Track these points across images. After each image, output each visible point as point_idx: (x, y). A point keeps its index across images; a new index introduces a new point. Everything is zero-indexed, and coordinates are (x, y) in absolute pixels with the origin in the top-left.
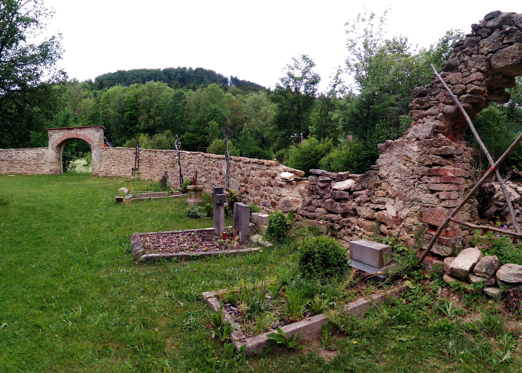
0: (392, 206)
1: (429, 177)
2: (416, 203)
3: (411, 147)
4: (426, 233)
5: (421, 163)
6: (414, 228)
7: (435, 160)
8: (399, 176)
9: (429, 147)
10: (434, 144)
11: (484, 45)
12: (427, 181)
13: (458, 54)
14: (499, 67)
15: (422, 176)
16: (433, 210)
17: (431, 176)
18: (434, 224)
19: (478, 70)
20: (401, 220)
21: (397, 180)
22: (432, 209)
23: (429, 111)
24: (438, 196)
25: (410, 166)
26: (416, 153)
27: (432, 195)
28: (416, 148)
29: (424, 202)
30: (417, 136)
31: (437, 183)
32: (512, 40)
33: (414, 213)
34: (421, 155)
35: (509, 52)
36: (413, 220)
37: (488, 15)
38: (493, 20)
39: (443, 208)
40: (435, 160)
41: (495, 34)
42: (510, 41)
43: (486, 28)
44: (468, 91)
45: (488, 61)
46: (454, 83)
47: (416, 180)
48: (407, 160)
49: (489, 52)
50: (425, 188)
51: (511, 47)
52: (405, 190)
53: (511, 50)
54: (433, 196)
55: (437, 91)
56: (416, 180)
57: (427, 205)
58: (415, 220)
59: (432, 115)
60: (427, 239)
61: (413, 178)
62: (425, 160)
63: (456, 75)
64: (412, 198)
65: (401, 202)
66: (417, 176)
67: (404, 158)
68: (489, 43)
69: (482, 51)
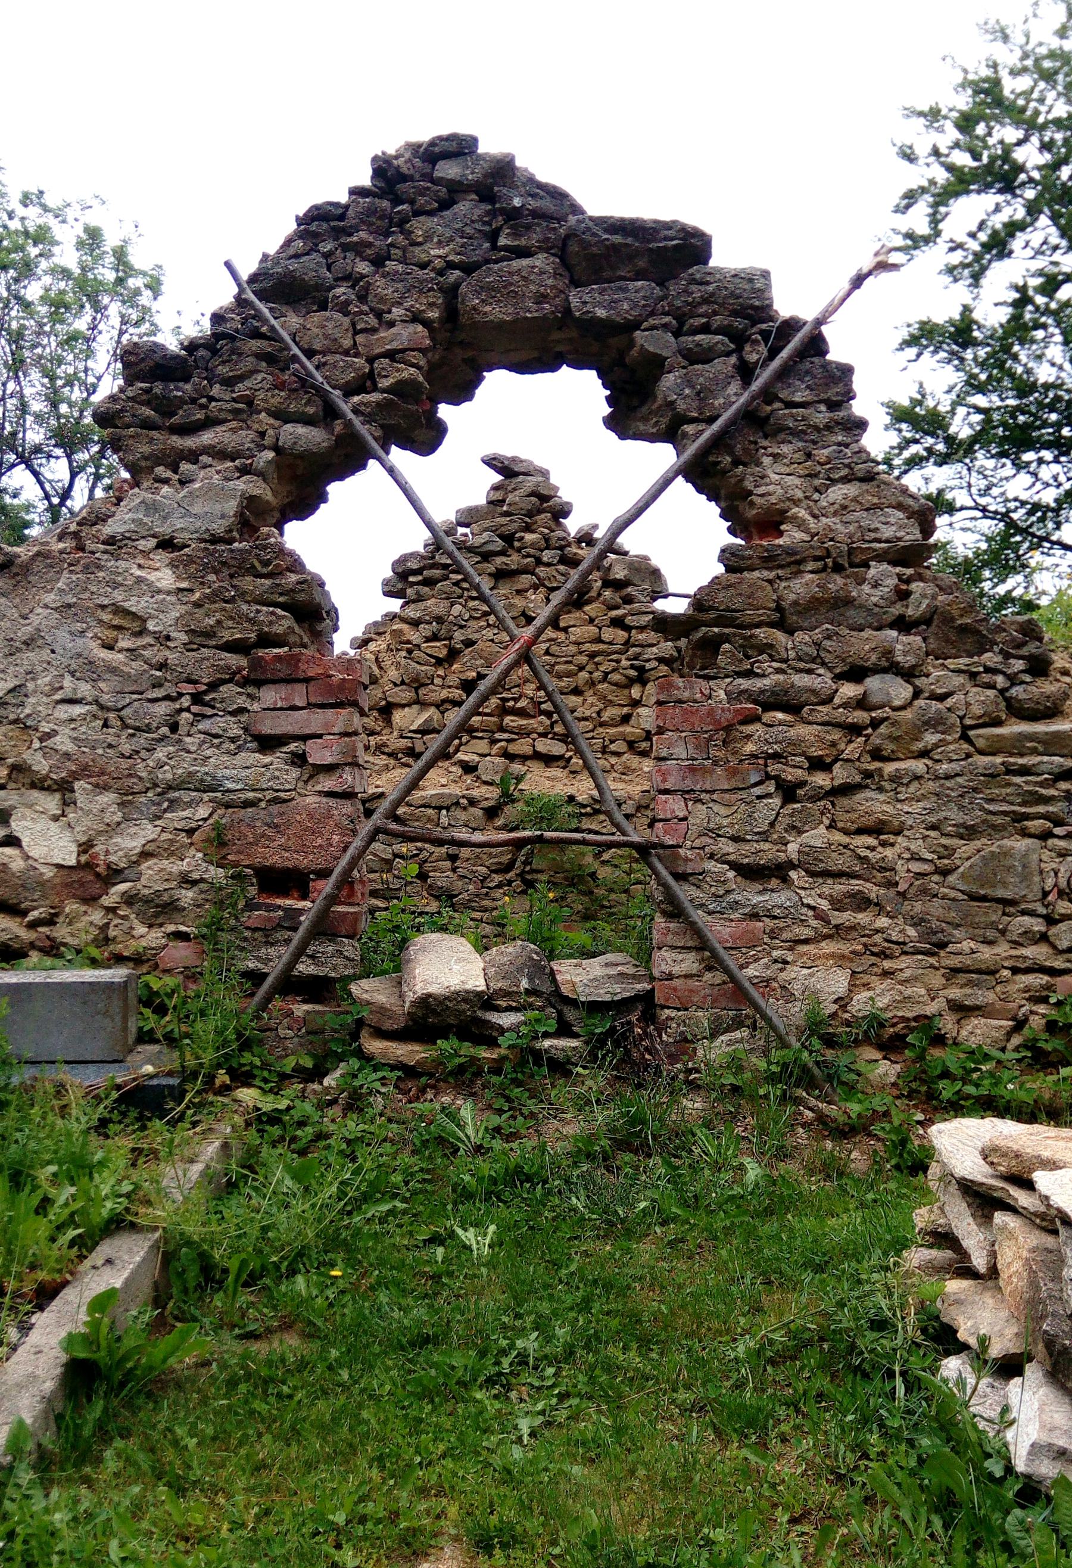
0: (54, 826)
1: (251, 690)
2: (186, 796)
3: (139, 573)
4: (250, 906)
5: (200, 637)
6: (187, 896)
7: (271, 623)
8: (85, 689)
9: (232, 576)
10: (257, 564)
11: (428, 238)
12: (241, 701)
13: (327, 246)
14: (492, 321)
15: (213, 686)
16: (282, 814)
17: (259, 684)
18: (289, 864)
19: (416, 318)
20: (114, 875)
21: (77, 710)
22: (275, 809)
23: (207, 437)
24: (299, 760)
25: (144, 647)
26: (172, 598)
27: (267, 759)
28: (165, 578)
29: (230, 785)
30: (164, 529)
31: (294, 708)
32: (533, 239)
33: (183, 838)
34: (197, 605)
35: (524, 278)
36: (177, 867)
37: (441, 138)
38: (460, 160)
39: (325, 800)
40: (271, 623)
41: (466, 207)
42: (523, 242)
43: (433, 181)
44: (384, 383)
45: (451, 292)
46: (317, 346)
47: (186, 701)
48: (119, 628)
49: (451, 265)
50: (235, 731)
51: (525, 262)
52: (126, 748)
53: (530, 273)
54: (276, 760)
55: (242, 367)
56: (186, 701)
57: (251, 795)
58: (193, 862)
59: (221, 454)
60: (255, 930)
61: (167, 698)
62: (219, 622)
63: (328, 319)
64: (169, 776)
65: (108, 798)
66: (189, 689)
67: (106, 617)
68: (448, 233)
69: (418, 254)
